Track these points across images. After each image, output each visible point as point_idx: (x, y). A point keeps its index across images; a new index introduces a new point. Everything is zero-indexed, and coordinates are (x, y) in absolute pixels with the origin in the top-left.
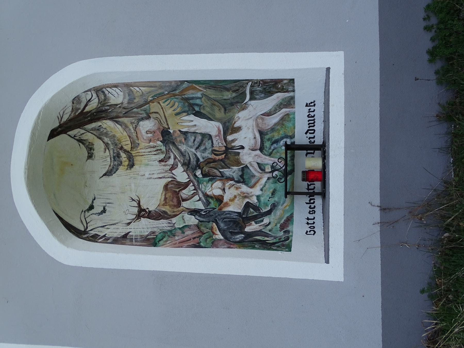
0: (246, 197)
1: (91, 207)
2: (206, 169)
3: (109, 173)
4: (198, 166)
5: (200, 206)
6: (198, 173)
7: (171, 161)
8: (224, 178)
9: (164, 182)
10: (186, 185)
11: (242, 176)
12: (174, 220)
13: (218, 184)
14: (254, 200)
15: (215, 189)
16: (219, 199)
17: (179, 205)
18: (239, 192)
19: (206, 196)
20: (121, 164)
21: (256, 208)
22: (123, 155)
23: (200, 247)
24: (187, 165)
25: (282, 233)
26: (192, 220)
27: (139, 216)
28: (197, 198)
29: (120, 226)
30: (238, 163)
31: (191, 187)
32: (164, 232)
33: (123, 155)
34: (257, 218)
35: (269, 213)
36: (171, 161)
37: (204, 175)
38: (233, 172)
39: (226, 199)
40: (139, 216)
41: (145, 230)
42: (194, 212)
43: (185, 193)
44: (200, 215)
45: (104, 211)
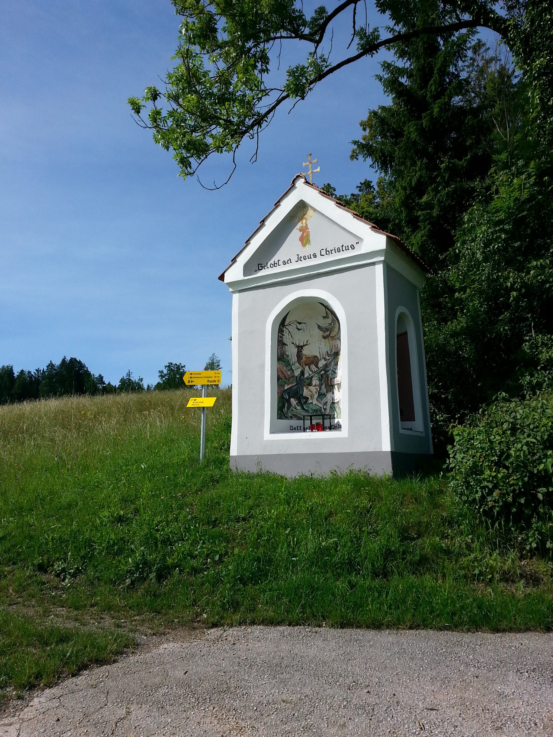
0: (311, 397)
1: (300, 323)
2: (324, 376)
3: (319, 327)
4: (326, 372)
5: (306, 375)
6: (323, 372)
7: (327, 358)
8: (321, 385)
9: (318, 355)
10: (317, 367)
11: (322, 394)
12: (297, 364)
13: (318, 383)
14: (310, 401)
15: (315, 382)
16: (310, 384)
17: (306, 365)
18: (314, 393)
19: (312, 377)
20: (325, 332)
21: (306, 402)
22: (328, 333)
23: (278, 380)
24: (326, 366)
25: (290, 415)
26: (297, 373)
27: (298, 347)
28: (311, 373)
29: (291, 340)
30: (327, 392)
31: (316, 369)
32: (288, 362)
33: (328, 333)
34: (300, 403)
35: (303, 409)
36: (327, 358)
37: (322, 375)
38: (324, 390)
39: (310, 387)
40: (298, 347)
41: (290, 352)
42: (302, 373)
43: (313, 367)
44: (300, 376)
45: (299, 330)
